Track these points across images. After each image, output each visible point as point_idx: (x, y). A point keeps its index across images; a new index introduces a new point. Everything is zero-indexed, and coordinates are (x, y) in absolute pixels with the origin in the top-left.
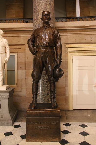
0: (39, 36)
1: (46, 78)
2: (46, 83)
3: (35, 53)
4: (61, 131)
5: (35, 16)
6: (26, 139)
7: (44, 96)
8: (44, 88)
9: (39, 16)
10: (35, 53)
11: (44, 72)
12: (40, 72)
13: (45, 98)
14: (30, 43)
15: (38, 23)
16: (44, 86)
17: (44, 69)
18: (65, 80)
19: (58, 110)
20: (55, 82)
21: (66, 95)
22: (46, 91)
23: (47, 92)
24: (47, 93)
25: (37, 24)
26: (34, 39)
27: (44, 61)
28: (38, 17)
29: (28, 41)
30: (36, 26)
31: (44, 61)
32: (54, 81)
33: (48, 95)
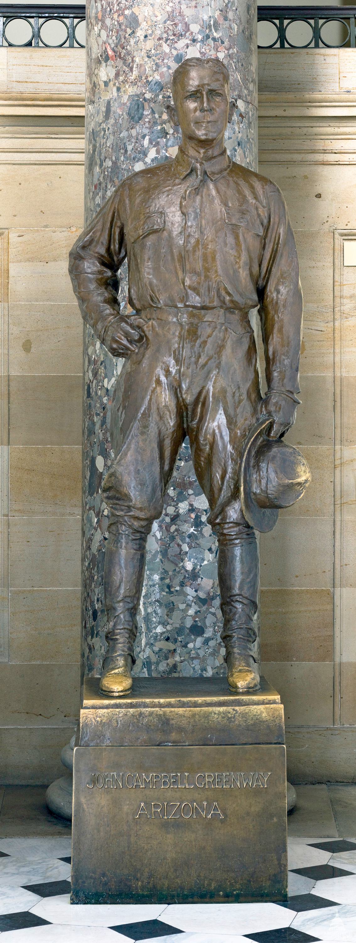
0: (152, 237)
1: (181, 511)
2: (185, 548)
3: (125, 342)
4: (290, 868)
5: (104, 26)
6: (69, 895)
7: (171, 646)
8: (169, 587)
9: (140, 33)
10: (125, 342)
11: (184, 467)
12: (162, 468)
13: (177, 658)
14: (91, 267)
15: (131, 90)
16: (170, 567)
17: (187, 437)
18: (329, 528)
19: (274, 702)
20: (69, 880)
21: (337, 660)
22: (182, 606)
23: (191, 612)
24: (189, 623)
25: (125, 99)
26: (115, 246)
27: (189, 398)
28: (132, 41)
29: (76, 257)
30: (116, 109)
31: (189, 398)
32: (248, 526)
33: (199, 640)
